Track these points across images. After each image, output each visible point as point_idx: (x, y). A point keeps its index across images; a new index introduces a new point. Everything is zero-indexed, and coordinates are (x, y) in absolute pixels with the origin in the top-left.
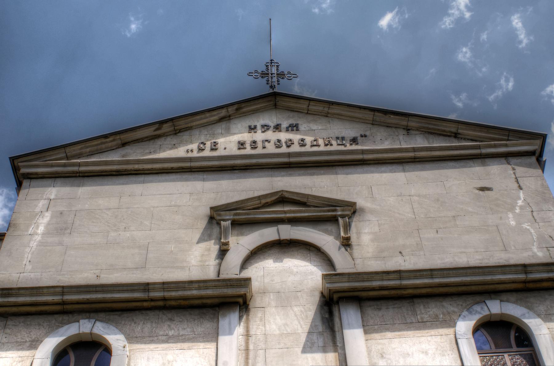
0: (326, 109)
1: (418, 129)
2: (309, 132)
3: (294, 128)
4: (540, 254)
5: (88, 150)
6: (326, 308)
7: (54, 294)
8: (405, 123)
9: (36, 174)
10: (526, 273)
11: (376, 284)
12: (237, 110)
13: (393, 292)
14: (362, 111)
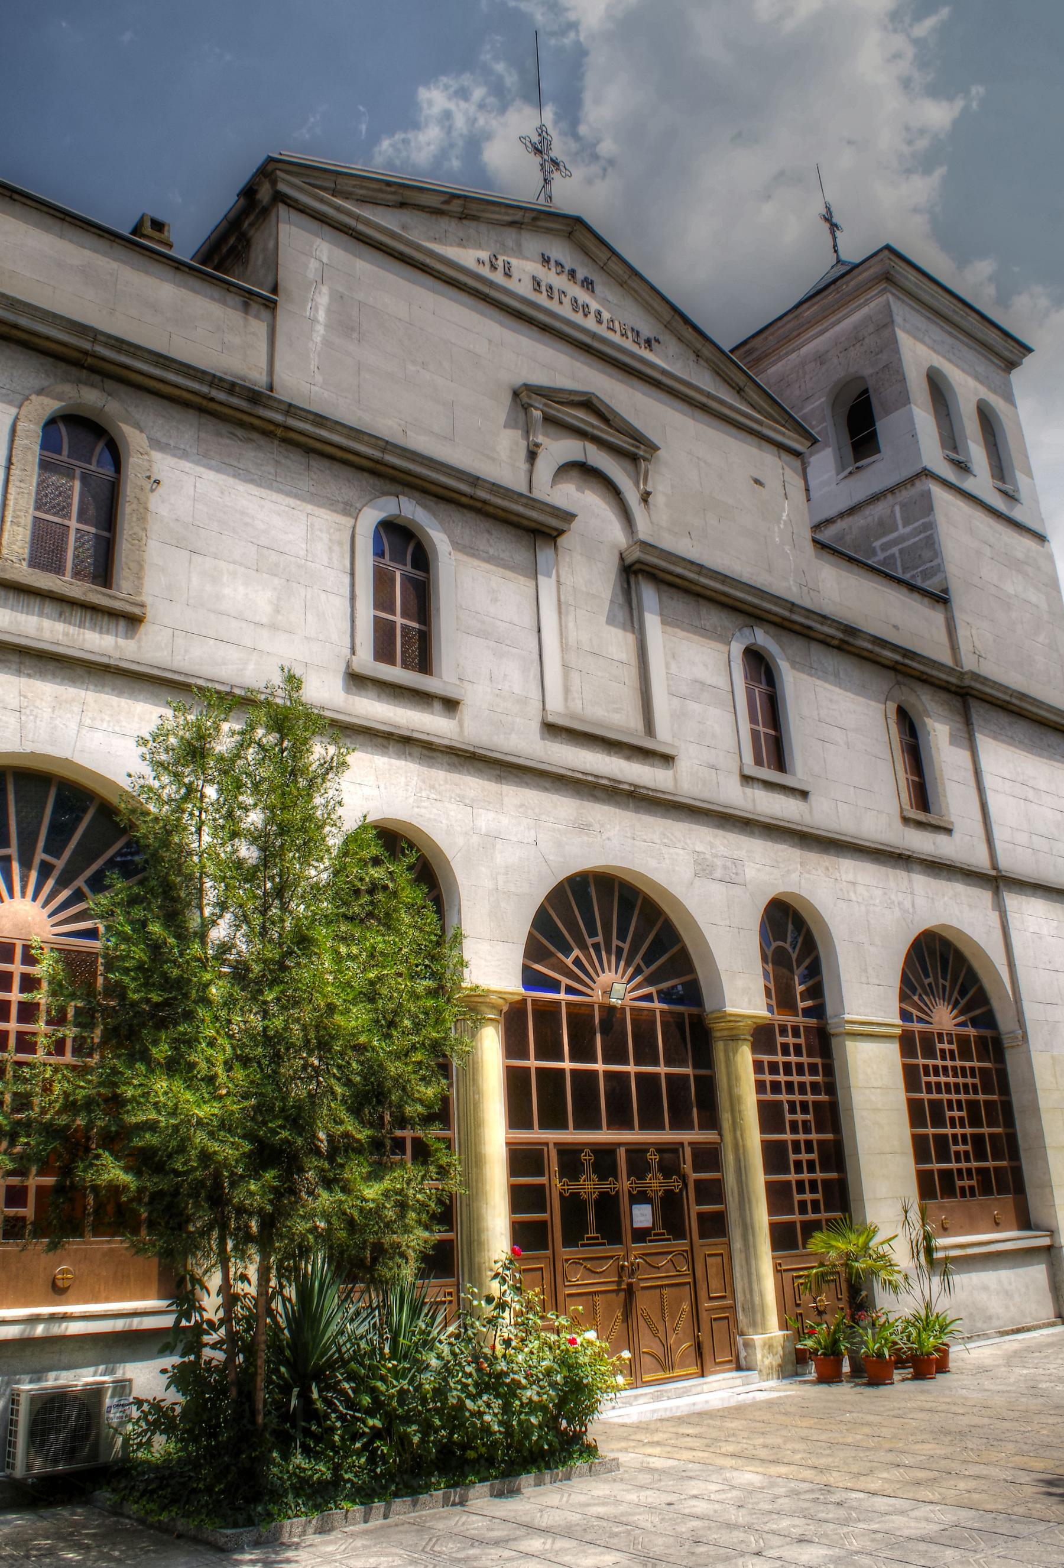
0: (626, 277)
1: (707, 361)
2: (604, 301)
3: (588, 284)
4: (794, 589)
5: (362, 192)
6: (624, 575)
7: (374, 447)
8: (699, 346)
9: (296, 201)
10: (791, 611)
11: (679, 570)
12: (535, 219)
13: (686, 584)
14: (663, 304)
